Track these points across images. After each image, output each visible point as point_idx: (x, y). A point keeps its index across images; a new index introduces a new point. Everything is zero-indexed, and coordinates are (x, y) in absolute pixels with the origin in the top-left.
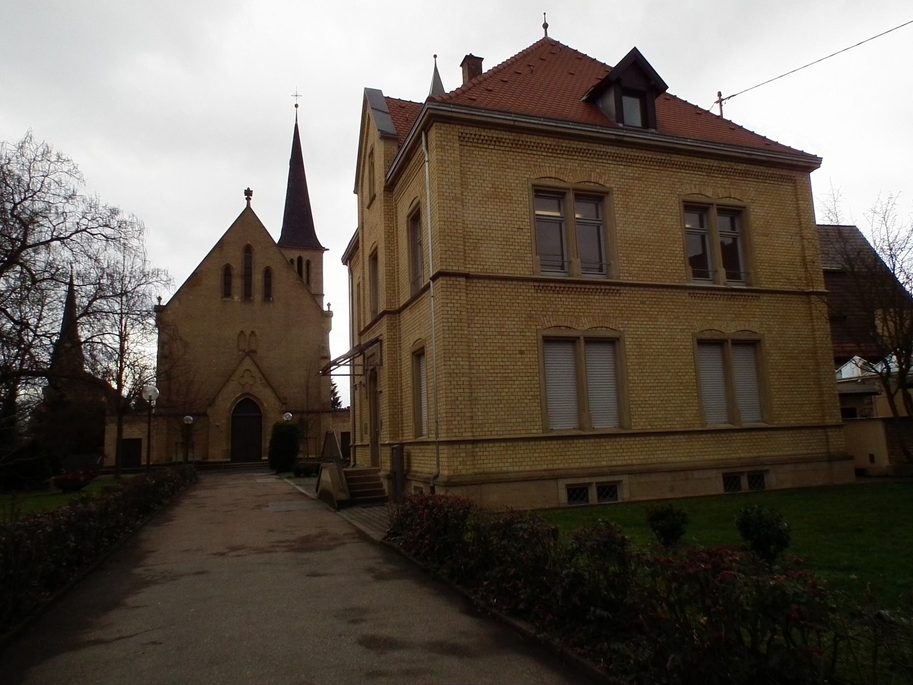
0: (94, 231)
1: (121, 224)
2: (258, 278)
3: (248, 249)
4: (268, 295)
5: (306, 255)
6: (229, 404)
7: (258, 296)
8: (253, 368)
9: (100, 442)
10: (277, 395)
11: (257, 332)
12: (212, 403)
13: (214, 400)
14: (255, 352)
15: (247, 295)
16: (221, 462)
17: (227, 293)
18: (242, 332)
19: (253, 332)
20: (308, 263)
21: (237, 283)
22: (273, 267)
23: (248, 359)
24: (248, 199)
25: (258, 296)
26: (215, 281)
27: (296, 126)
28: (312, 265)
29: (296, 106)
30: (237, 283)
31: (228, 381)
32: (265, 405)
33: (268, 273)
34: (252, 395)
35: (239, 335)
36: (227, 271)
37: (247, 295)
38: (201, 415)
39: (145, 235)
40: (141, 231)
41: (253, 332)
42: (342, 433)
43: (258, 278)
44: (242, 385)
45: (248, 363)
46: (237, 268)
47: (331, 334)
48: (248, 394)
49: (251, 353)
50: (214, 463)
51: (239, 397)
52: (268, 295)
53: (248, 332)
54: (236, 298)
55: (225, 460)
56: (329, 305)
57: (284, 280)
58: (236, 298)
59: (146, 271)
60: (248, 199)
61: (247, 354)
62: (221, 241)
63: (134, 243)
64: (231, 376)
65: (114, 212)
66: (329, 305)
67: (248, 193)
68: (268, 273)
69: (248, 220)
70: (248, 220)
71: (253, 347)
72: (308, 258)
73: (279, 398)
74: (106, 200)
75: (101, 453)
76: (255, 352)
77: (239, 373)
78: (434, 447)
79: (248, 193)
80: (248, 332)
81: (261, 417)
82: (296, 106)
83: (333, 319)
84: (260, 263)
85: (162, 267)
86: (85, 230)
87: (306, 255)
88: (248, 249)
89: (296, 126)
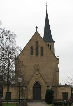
0: (4, 37)
1: (10, 35)
2: (39, 49)
3: (37, 42)
4: (42, 54)
5: (50, 44)
6: (33, 84)
7: (39, 55)
8: (39, 74)
9: (2, 93)
10: (45, 81)
11: (39, 64)
12: (28, 83)
13: (29, 83)
14: (39, 69)
15: (37, 54)
16: (31, 100)
17: (32, 54)
18: (36, 64)
19: (38, 64)
20: (50, 46)
21: (34, 51)
22: (43, 47)
23: (37, 72)
24: (37, 29)
25: (39, 55)
26: (29, 51)
27: (47, 11)
28: (52, 46)
29: (47, 6)
30: (34, 51)
31: (32, 77)
32: (42, 84)
33: (42, 48)
34: (38, 81)
35: (35, 65)
36: (32, 47)
37: (37, 54)
38: (26, 87)
39: (16, 38)
40: (15, 37)
41: (38, 64)
42: (63, 93)
43: (39, 49)
44: (36, 79)
45: (37, 72)
46: (34, 48)
47: (59, 65)
48: (37, 81)
49: (38, 70)
50: (29, 100)
51: (35, 82)
52: (42, 54)
53: (37, 64)
54: (34, 55)
55: (32, 99)
56: (58, 56)
57: (46, 49)
58: (34, 55)
59: (15, 47)
60: (37, 29)
61: (37, 70)
62: (30, 40)
63: (13, 40)
64: (33, 76)
65: (9, 32)
66: (58, 56)
67: (37, 28)
68: (42, 48)
69: (37, 34)
70: (37, 34)
71: (38, 68)
72: (50, 44)
73: (45, 82)
74: (7, 29)
75: (2, 96)
76: (39, 69)
77: (35, 75)
78: (57, 99)
79: (37, 28)
80: (37, 64)
81: (41, 87)
82: (47, 6)
83: (59, 60)
84: (40, 45)
85: (19, 46)
86: (2, 37)
87: (50, 44)
88: (37, 42)
89: (47, 11)
